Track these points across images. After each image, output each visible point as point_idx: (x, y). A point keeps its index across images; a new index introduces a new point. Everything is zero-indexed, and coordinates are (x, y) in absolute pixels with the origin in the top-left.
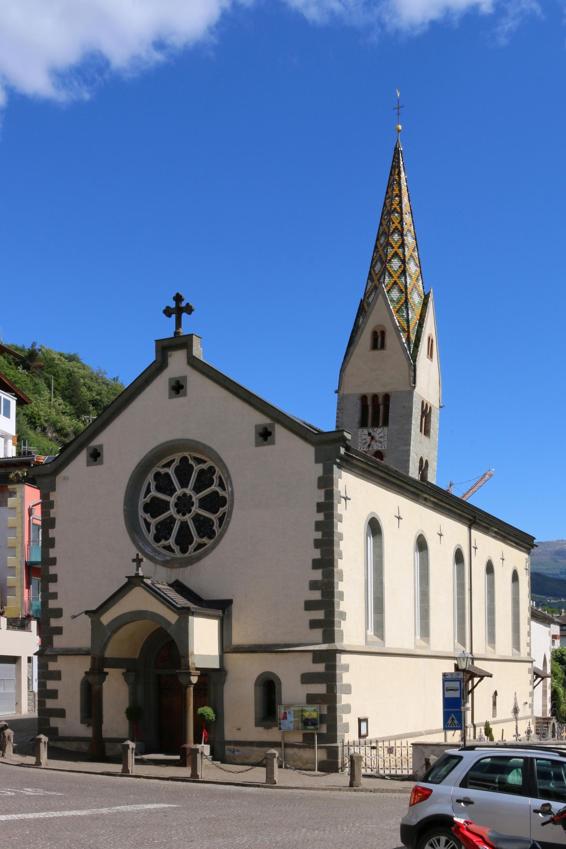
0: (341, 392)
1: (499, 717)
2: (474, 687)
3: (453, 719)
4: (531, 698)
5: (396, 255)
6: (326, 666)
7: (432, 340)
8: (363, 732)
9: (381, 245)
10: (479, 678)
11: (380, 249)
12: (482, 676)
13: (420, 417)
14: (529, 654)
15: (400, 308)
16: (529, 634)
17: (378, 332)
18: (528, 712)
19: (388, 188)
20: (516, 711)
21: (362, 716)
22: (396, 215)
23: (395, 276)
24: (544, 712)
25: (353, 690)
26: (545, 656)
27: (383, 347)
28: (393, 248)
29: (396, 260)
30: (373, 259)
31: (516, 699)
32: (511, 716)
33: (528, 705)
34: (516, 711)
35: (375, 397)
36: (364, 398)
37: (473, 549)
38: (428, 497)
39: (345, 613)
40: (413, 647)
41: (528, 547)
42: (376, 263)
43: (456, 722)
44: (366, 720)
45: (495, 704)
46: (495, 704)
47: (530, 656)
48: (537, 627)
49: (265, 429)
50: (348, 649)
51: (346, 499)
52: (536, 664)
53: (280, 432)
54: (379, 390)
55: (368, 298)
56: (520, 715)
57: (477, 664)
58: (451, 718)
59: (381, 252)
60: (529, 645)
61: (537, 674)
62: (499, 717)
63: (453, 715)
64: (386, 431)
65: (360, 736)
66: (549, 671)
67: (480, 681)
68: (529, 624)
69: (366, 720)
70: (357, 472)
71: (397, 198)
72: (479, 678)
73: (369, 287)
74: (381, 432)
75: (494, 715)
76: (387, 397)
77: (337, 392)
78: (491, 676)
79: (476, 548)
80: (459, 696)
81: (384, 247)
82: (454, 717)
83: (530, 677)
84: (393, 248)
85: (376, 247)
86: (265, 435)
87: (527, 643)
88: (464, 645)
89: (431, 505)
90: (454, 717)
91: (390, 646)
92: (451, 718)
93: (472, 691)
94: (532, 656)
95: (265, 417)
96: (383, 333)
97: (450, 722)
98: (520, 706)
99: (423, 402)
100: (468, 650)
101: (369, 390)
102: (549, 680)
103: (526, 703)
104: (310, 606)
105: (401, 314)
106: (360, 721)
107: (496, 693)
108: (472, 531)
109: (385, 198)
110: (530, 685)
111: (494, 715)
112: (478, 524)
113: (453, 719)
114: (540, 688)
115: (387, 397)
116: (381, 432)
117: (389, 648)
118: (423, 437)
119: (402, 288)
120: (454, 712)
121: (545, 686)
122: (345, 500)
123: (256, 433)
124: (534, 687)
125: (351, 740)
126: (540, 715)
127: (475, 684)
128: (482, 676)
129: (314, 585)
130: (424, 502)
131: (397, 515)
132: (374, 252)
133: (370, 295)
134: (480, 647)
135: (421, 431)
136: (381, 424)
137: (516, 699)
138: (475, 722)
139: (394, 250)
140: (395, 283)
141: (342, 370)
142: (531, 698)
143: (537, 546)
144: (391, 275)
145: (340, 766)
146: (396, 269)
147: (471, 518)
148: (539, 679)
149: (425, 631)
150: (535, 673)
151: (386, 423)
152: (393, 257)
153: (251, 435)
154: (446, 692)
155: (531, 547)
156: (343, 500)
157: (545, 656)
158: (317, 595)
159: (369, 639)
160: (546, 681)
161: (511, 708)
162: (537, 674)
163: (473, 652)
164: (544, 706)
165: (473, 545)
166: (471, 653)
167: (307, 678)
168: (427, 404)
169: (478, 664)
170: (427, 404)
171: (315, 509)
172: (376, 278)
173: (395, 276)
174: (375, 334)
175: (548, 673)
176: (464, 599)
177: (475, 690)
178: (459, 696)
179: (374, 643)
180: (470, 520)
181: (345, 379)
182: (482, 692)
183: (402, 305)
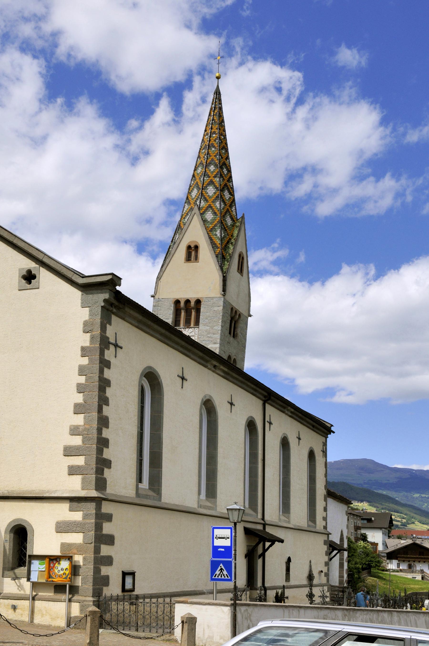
0: (157, 297)
1: (293, 582)
2: (265, 550)
3: (221, 569)
4: (327, 567)
5: (211, 183)
6: (83, 514)
7: (243, 258)
8: (128, 586)
9: (198, 174)
10: (270, 543)
11: (197, 177)
12: (274, 540)
13: (229, 321)
14: (325, 528)
15: (213, 228)
16: (325, 509)
17: (192, 246)
18: (324, 580)
19: (206, 126)
20: (310, 577)
21: (127, 569)
22: (213, 149)
23: (210, 201)
24: (341, 582)
25: (116, 541)
26: (342, 532)
27: (196, 258)
28: (209, 177)
29: (211, 187)
30: (190, 186)
31: (310, 566)
32: (305, 582)
33: (323, 574)
34: (310, 577)
35: (188, 302)
36: (177, 302)
37: (267, 425)
38: (217, 364)
39: (111, 461)
40: (195, 506)
41: (326, 431)
42: (193, 189)
43: (225, 572)
44: (133, 574)
45: (288, 569)
46: (288, 569)
47: (326, 529)
48: (332, 504)
49: (29, 271)
50: (110, 498)
51: (116, 346)
52: (331, 538)
53: (44, 275)
54: (192, 296)
55: (184, 218)
56: (315, 582)
57: (269, 530)
58: (219, 568)
59: (198, 180)
60: (325, 519)
61: (332, 547)
62: (293, 582)
63: (221, 565)
64: (197, 331)
65: (124, 590)
66: (346, 546)
67: (270, 546)
68: (325, 500)
69: (133, 574)
70: (133, 322)
71: (214, 135)
72: (270, 543)
73: (185, 209)
74: (192, 332)
75: (288, 578)
76: (198, 302)
77: (152, 296)
78: (282, 541)
79: (270, 423)
80: (230, 545)
81: (201, 176)
82: (223, 567)
83: (325, 548)
84: (209, 177)
85: (194, 176)
86: (29, 277)
87: (323, 517)
88: (255, 510)
89: (222, 374)
90: (223, 567)
91: (167, 501)
92: (219, 568)
93: (263, 555)
94: (328, 530)
95: (30, 261)
96: (196, 247)
97: (218, 572)
98: (315, 573)
99: (232, 309)
100: (260, 516)
101: (183, 296)
102: (346, 554)
103: (322, 571)
104: (69, 452)
105: (214, 233)
106: (124, 574)
107: (289, 560)
108: (267, 406)
109: (204, 135)
110: (326, 555)
111: (288, 578)
112: (274, 401)
113: (221, 569)
114: (336, 561)
115: (198, 302)
116: (192, 332)
117: (166, 503)
118: (232, 339)
119: (216, 211)
120: (224, 563)
121: (341, 559)
122: (116, 348)
123: (19, 277)
124: (331, 559)
125: (115, 594)
126: (337, 584)
127: (266, 547)
128: (274, 540)
129: (74, 431)
130: (213, 369)
131: (181, 375)
132: (192, 180)
133: (186, 216)
134: (272, 512)
135: (230, 333)
136: (192, 325)
137: (310, 566)
138: (267, 585)
139: (210, 179)
140: (210, 207)
141: (159, 278)
142: (327, 567)
143: (334, 432)
144: (206, 200)
145: (89, 619)
146: (211, 195)
147: (266, 394)
148: (335, 552)
149: (211, 491)
150: (330, 546)
151: (197, 323)
152: (208, 184)
153: (16, 279)
154: (215, 540)
155: (328, 433)
156: (112, 348)
157: (342, 532)
158: (77, 441)
159: (140, 492)
160: (343, 555)
161: (306, 574)
162: (332, 547)
163: (266, 518)
164: (341, 576)
165: (267, 419)
166: (263, 519)
167: (63, 528)
168: (236, 311)
169: (269, 530)
170: (236, 311)
171: (79, 353)
172: (192, 202)
173: (210, 201)
174: (189, 247)
175: (181, 306)
176: (256, 468)
177: (267, 553)
178: (230, 545)
179: (146, 497)
180: (265, 397)
181: (161, 284)
182: (275, 556)
183: (215, 225)
